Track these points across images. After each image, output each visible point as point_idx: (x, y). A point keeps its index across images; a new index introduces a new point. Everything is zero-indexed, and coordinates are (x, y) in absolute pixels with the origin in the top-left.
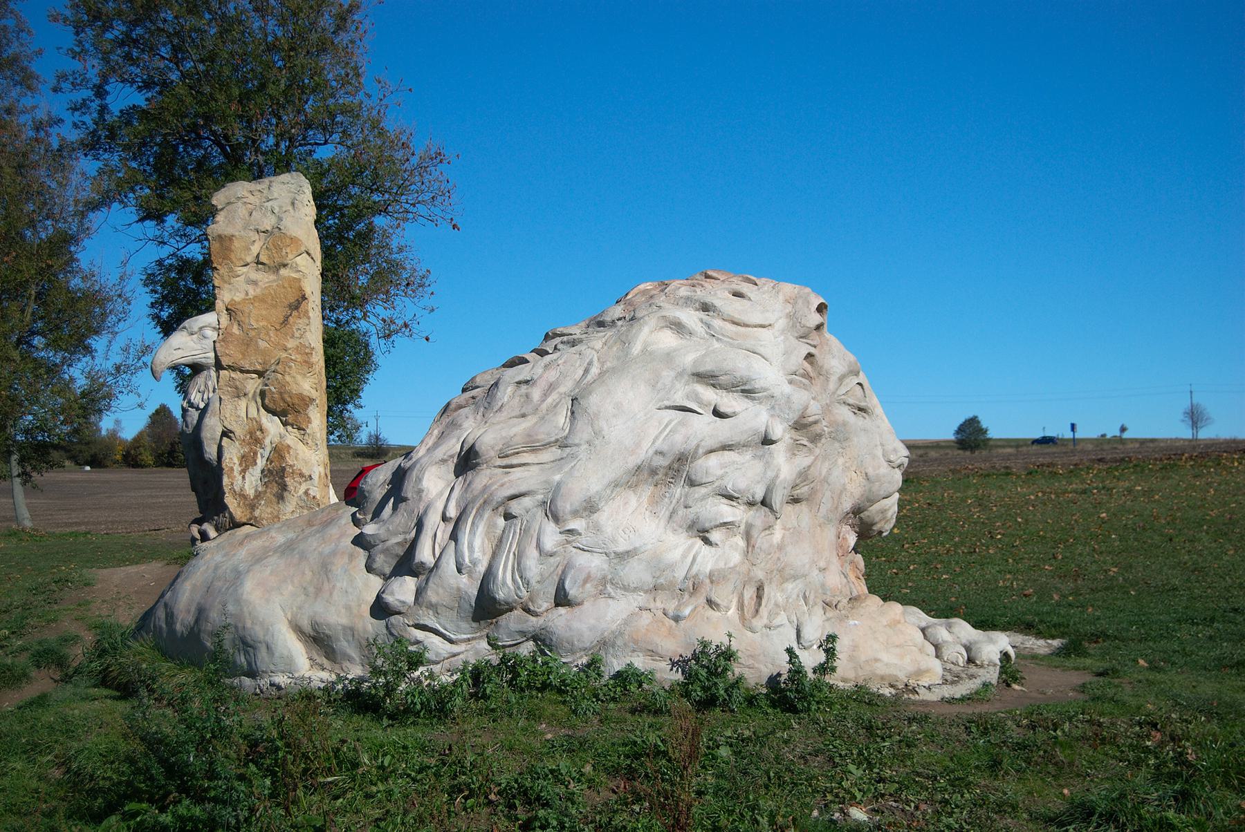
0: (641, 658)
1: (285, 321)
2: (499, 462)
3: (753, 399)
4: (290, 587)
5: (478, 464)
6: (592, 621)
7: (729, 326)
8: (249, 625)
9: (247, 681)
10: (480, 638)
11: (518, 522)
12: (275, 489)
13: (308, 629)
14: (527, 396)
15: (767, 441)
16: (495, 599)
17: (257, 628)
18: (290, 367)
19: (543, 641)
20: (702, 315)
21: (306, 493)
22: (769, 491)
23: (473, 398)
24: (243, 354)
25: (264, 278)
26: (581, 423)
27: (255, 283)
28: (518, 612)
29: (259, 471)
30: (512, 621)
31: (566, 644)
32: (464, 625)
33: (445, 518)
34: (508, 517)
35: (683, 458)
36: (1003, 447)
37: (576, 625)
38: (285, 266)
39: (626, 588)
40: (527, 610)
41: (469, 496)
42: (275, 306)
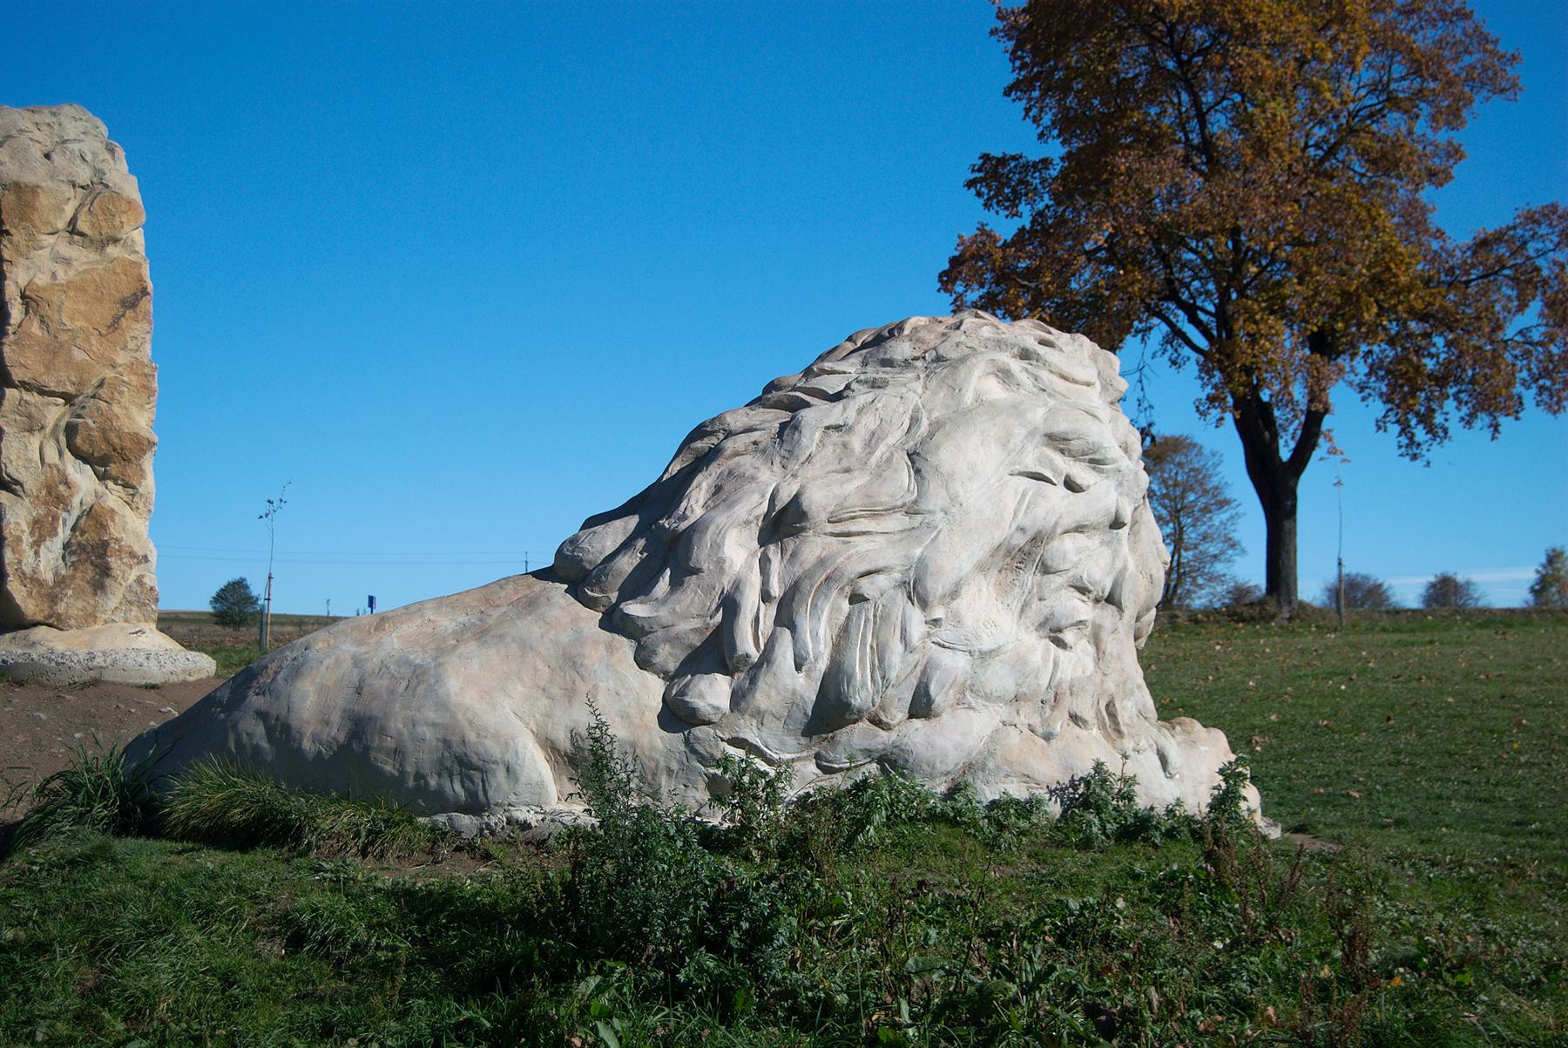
0: (1015, 785)
1: (115, 324)
2: (830, 528)
3: (1101, 471)
4: (520, 688)
5: (803, 529)
6: (958, 738)
7: (1056, 379)
8: (472, 737)
9: (465, 821)
10: (805, 758)
11: (870, 606)
12: (91, 573)
13: (565, 744)
14: (845, 446)
15: (1117, 524)
16: (849, 705)
17: (489, 743)
18: (121, 393)
19: (894, 764)
20: (1024, 363)
21: (139, 580)
22: (1116, 584)
23: (755, 443)
24: (47, 367)
25: (81, 256)
26: (935, 489)
27: (67, 262)
28: (864, 725)
29: (60, 546)
30: (858, 735)
31: (925, 767)
32: (791, 741)
33: (766, 596)
34: (856, 598)
35: (1038, 539)
36: (282, 624)
37: (939, 742)
38: (116, 241)
39: (987, 697)
40: (877, 722)
41: (798, 570)
42: (100, 300)
